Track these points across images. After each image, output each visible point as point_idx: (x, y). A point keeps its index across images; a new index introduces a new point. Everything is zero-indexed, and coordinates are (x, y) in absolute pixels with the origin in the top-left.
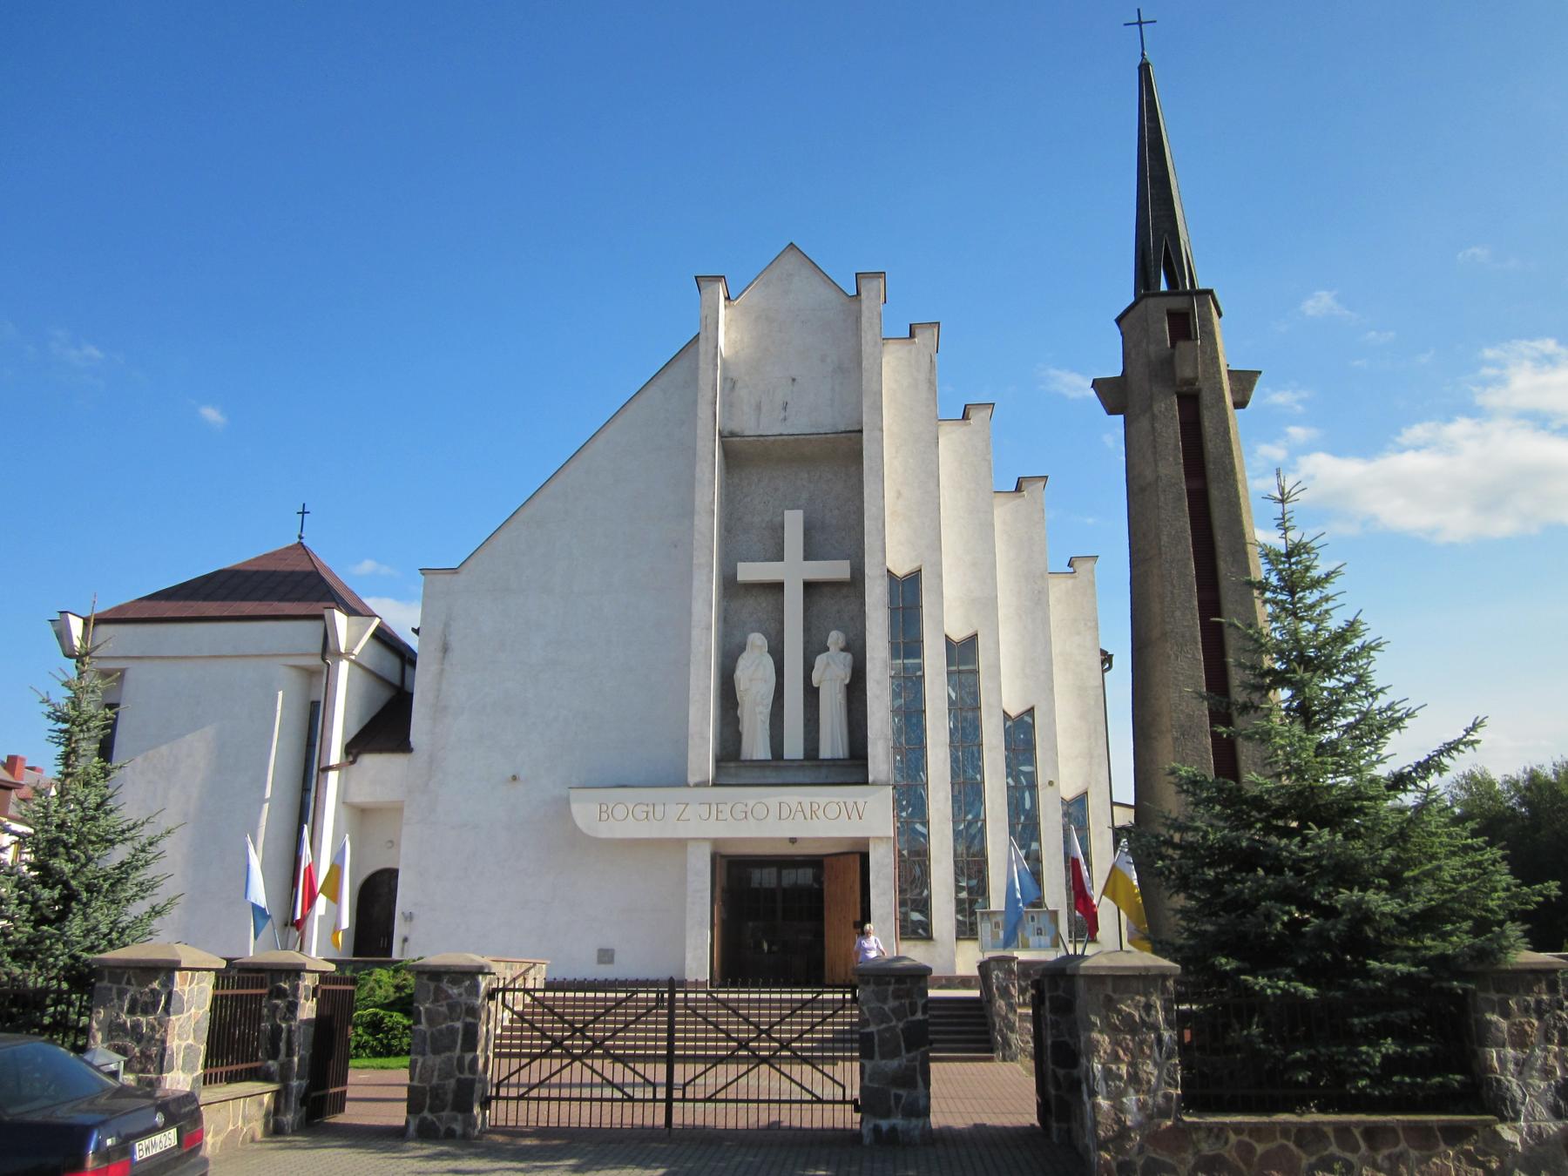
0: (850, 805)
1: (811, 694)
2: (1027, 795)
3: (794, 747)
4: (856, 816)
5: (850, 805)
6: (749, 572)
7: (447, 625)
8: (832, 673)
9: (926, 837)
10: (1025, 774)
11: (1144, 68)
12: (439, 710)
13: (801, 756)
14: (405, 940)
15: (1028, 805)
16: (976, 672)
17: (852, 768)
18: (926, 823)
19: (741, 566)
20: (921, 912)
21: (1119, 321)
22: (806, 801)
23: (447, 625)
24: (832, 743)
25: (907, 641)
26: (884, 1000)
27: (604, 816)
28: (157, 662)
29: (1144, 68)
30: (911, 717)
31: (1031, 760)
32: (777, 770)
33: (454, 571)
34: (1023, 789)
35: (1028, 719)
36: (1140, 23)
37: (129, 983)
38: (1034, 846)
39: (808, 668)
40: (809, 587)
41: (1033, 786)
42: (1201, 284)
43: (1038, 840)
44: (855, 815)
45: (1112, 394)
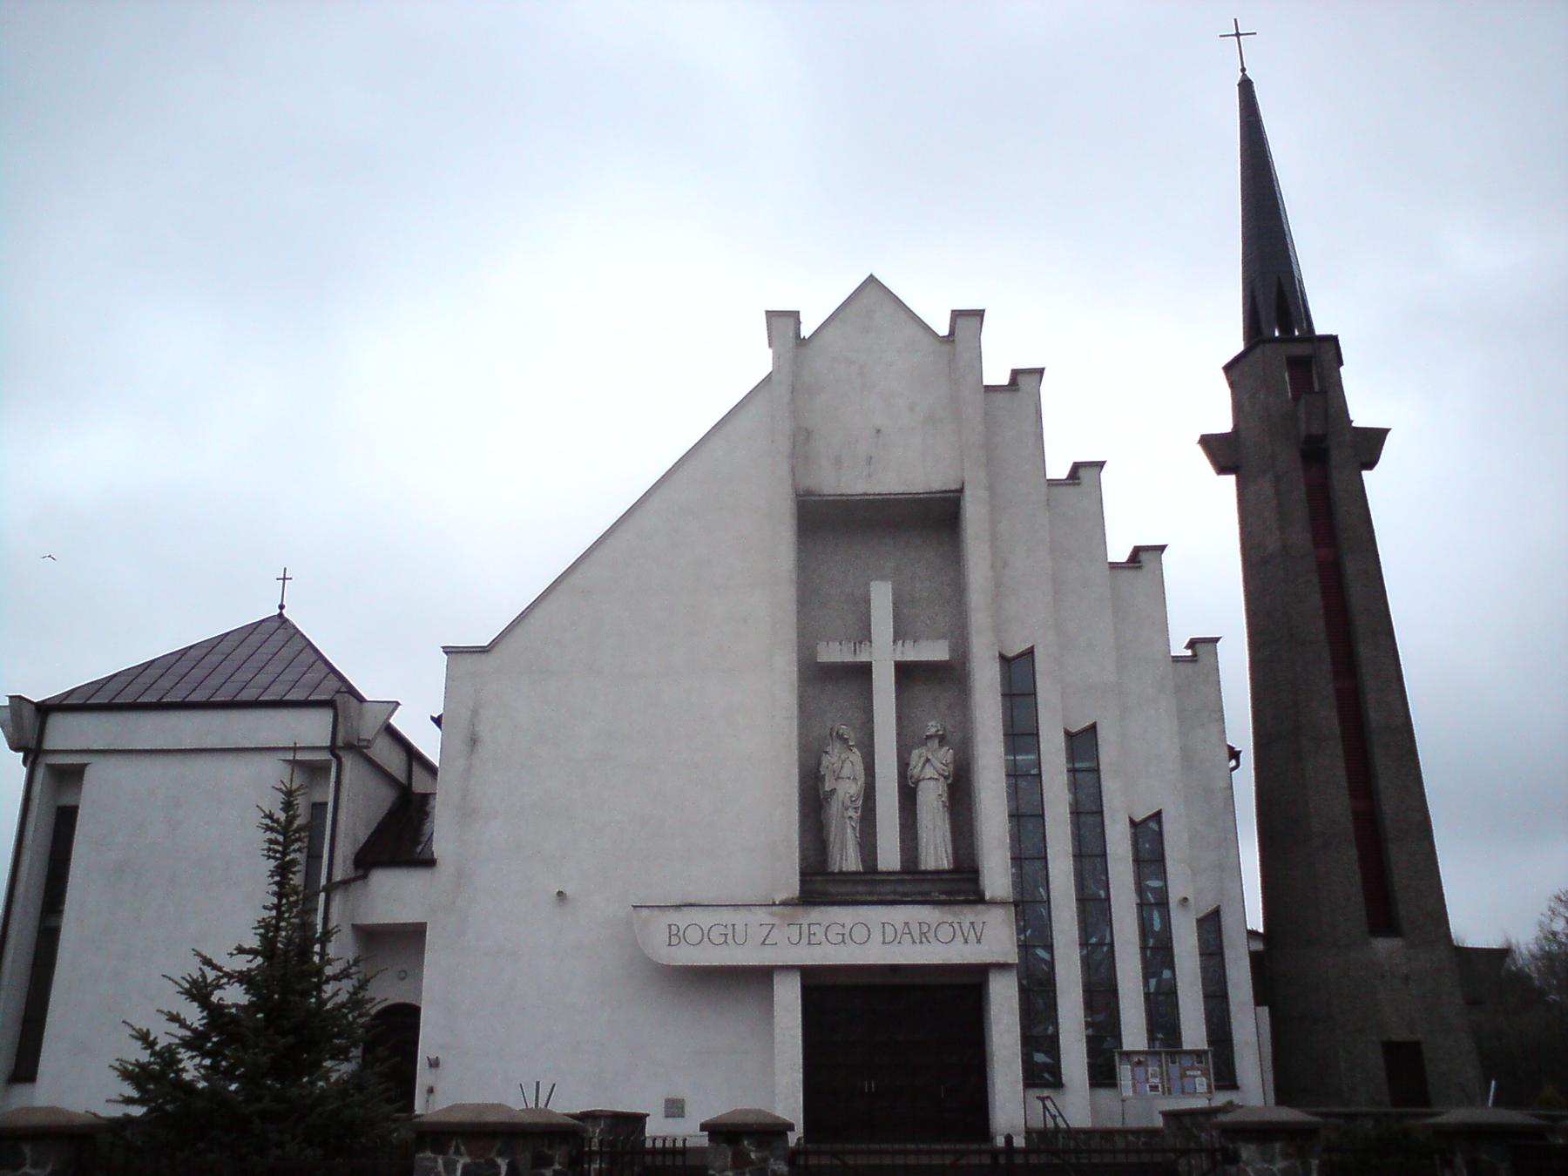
0: (966, 925)
1: (908, 794)
2: (1156, 915)
3: (889, 857)
4: (983, 938)
5: (966, 925)
6: (833, 653)
7: (475, 713)
8: (932, 768)
9: (1051, 964)
10: (1154, 889)
11: (1246, 87)
12: (467, 813)
13: (897, 867)
14: (431, 1091)
15: (1157, 926)
16: (1096, 770)
17: (960, 885)
18: (1050, 948)
19: (821, 646)
20: (1046, 1053)
21: (1229, 369)
22: (978, 921)
23: (475, 713)
24: (936, 853)
25: (1021, 735)
26: (1272, 1161)
27: (675, 940)
28: (229, 758)
29: (1246, 87)
30: (1026, 820)
31: (1162, 874)
32: (870, 887)
33: (483, 650)
34: (1153, 903)
35: (1154, 826)
36: (1238, 35)
37: (457, 1152)
38: (1166, 974)
39: (903, 766)
40: (906, 673)
41: (1163, 904)
42: (1320, 329)
43: (1172, 966)
44: (972, 937)
45: (1370, 444)
